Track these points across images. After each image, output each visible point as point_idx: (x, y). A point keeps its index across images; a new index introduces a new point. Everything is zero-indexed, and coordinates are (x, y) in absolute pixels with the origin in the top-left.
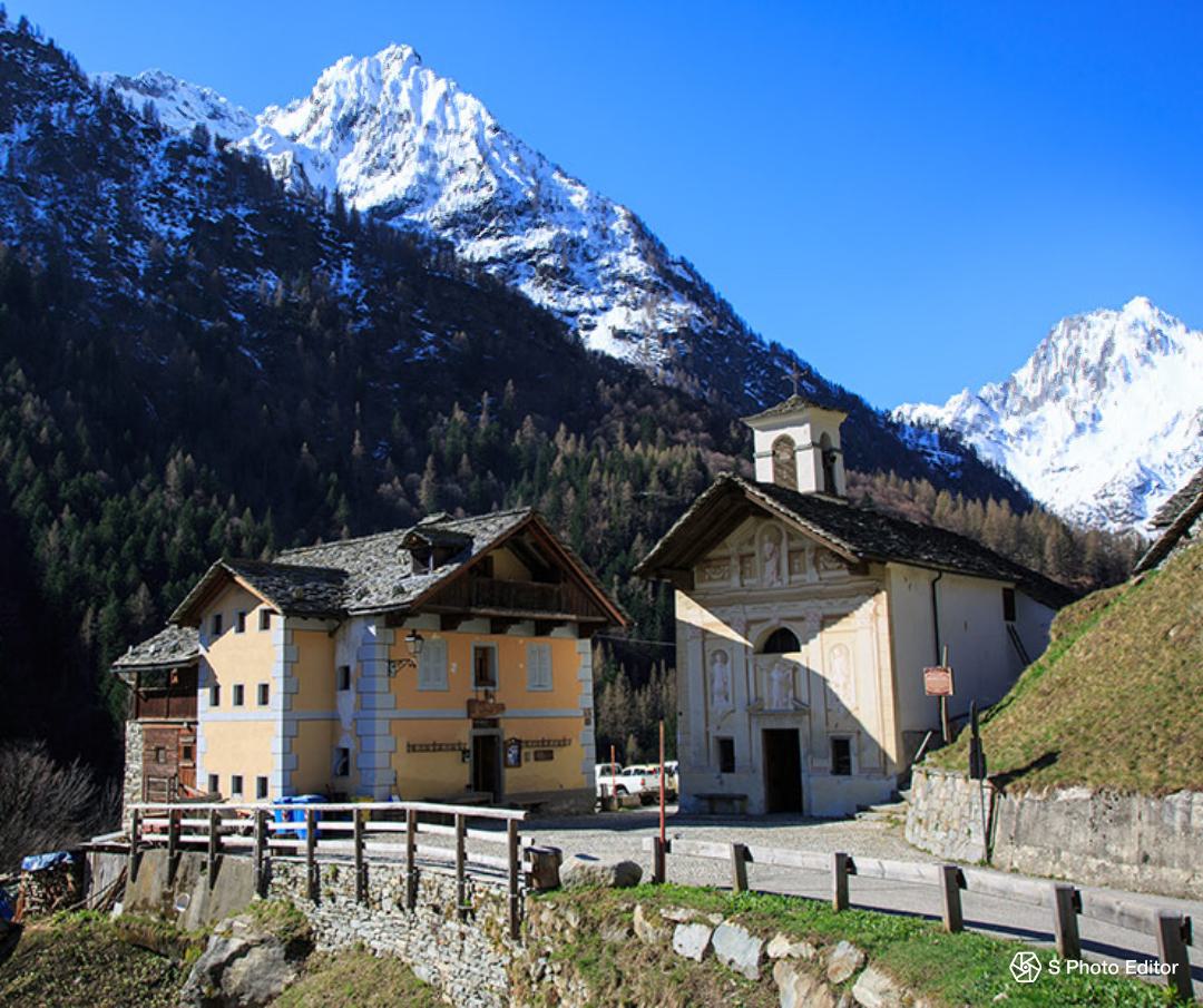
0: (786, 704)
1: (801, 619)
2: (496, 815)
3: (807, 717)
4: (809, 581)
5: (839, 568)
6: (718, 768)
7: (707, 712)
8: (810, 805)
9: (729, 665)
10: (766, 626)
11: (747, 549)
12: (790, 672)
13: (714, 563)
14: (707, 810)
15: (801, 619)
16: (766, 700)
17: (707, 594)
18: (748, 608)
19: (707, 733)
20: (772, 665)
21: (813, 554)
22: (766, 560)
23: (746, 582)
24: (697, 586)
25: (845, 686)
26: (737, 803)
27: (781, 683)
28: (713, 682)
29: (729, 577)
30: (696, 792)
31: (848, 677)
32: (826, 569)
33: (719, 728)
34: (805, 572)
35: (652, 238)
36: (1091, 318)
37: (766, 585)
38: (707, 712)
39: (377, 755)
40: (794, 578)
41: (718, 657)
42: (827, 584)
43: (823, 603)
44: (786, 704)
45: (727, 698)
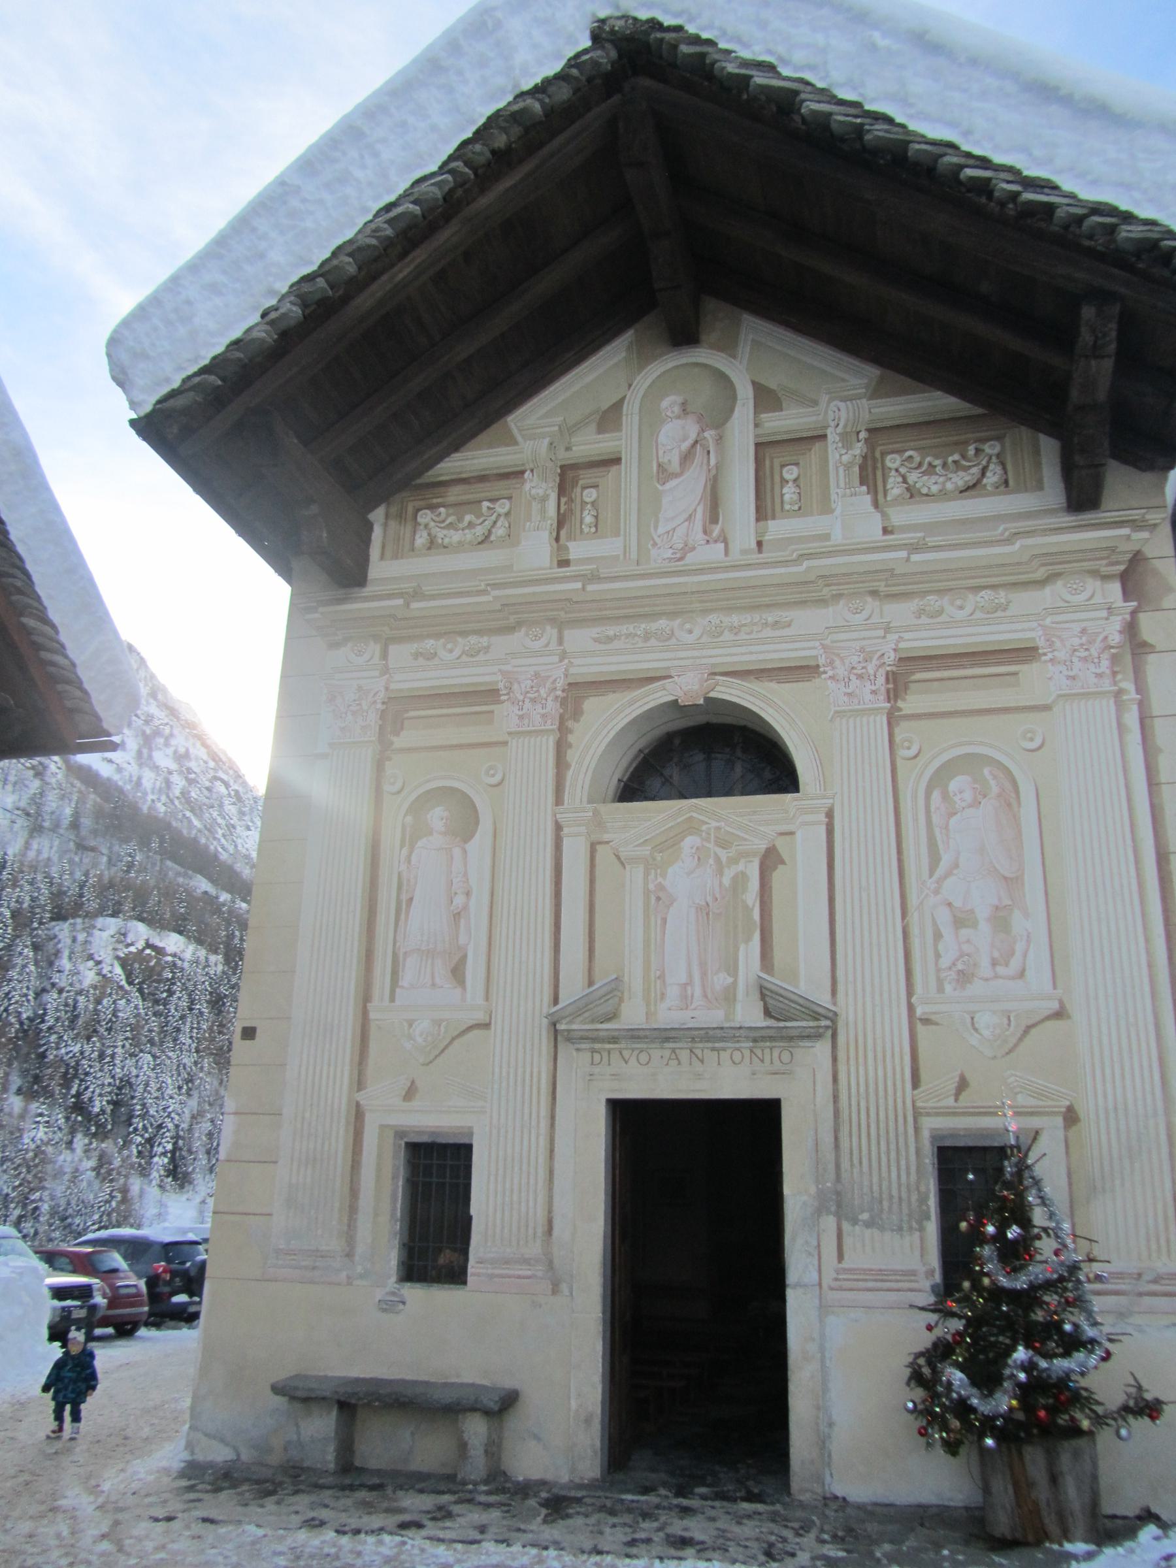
0: (729, 996)
1: (804, 671)
2: (987, 640)
3: (822, 1049)
4: (837, 537)
5: (970, 489)
6: (392, 1258)
7: (249, 1214)
8: (823, 1443)
9: (480, 842)
10: (657, 696)
11: (589, 445)
12: (753, 871)
13: (454, 494)
14: (329, 1457)
15: (804, 671)
16: (635, 980)
17: (417, 594)
18: (578, 638)
19: (359, 1115)
20: (669, 844)
21: (859, 449)
22: (664, 474)
23: (576, 550)
24: (379, 568)
25: (1001, 920)
26: (476, 1429)
27: (704, 911)
28: (403, 907)
29: (511, 538)
30: (281, 1375)
31: (1013, 882)
32: (912, 493)
33: (410, 1093)
34: (826, 508)
35: (475, 1504)
36: (701, 702)
37: (660, 556)
38: (249, 1214)
39: (1164, 787)
40: (776, 528)
41: (437, 816)
42: (915, 548)
43: (900, 612)
44: (729, 996)
45: (458, 973)
